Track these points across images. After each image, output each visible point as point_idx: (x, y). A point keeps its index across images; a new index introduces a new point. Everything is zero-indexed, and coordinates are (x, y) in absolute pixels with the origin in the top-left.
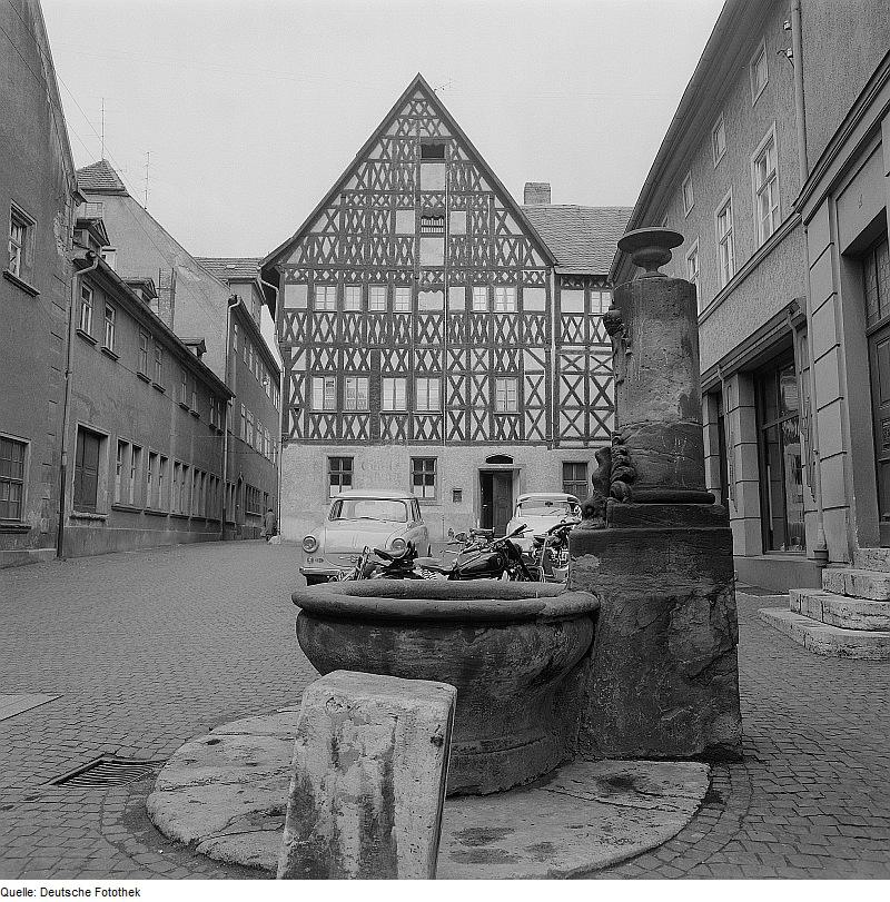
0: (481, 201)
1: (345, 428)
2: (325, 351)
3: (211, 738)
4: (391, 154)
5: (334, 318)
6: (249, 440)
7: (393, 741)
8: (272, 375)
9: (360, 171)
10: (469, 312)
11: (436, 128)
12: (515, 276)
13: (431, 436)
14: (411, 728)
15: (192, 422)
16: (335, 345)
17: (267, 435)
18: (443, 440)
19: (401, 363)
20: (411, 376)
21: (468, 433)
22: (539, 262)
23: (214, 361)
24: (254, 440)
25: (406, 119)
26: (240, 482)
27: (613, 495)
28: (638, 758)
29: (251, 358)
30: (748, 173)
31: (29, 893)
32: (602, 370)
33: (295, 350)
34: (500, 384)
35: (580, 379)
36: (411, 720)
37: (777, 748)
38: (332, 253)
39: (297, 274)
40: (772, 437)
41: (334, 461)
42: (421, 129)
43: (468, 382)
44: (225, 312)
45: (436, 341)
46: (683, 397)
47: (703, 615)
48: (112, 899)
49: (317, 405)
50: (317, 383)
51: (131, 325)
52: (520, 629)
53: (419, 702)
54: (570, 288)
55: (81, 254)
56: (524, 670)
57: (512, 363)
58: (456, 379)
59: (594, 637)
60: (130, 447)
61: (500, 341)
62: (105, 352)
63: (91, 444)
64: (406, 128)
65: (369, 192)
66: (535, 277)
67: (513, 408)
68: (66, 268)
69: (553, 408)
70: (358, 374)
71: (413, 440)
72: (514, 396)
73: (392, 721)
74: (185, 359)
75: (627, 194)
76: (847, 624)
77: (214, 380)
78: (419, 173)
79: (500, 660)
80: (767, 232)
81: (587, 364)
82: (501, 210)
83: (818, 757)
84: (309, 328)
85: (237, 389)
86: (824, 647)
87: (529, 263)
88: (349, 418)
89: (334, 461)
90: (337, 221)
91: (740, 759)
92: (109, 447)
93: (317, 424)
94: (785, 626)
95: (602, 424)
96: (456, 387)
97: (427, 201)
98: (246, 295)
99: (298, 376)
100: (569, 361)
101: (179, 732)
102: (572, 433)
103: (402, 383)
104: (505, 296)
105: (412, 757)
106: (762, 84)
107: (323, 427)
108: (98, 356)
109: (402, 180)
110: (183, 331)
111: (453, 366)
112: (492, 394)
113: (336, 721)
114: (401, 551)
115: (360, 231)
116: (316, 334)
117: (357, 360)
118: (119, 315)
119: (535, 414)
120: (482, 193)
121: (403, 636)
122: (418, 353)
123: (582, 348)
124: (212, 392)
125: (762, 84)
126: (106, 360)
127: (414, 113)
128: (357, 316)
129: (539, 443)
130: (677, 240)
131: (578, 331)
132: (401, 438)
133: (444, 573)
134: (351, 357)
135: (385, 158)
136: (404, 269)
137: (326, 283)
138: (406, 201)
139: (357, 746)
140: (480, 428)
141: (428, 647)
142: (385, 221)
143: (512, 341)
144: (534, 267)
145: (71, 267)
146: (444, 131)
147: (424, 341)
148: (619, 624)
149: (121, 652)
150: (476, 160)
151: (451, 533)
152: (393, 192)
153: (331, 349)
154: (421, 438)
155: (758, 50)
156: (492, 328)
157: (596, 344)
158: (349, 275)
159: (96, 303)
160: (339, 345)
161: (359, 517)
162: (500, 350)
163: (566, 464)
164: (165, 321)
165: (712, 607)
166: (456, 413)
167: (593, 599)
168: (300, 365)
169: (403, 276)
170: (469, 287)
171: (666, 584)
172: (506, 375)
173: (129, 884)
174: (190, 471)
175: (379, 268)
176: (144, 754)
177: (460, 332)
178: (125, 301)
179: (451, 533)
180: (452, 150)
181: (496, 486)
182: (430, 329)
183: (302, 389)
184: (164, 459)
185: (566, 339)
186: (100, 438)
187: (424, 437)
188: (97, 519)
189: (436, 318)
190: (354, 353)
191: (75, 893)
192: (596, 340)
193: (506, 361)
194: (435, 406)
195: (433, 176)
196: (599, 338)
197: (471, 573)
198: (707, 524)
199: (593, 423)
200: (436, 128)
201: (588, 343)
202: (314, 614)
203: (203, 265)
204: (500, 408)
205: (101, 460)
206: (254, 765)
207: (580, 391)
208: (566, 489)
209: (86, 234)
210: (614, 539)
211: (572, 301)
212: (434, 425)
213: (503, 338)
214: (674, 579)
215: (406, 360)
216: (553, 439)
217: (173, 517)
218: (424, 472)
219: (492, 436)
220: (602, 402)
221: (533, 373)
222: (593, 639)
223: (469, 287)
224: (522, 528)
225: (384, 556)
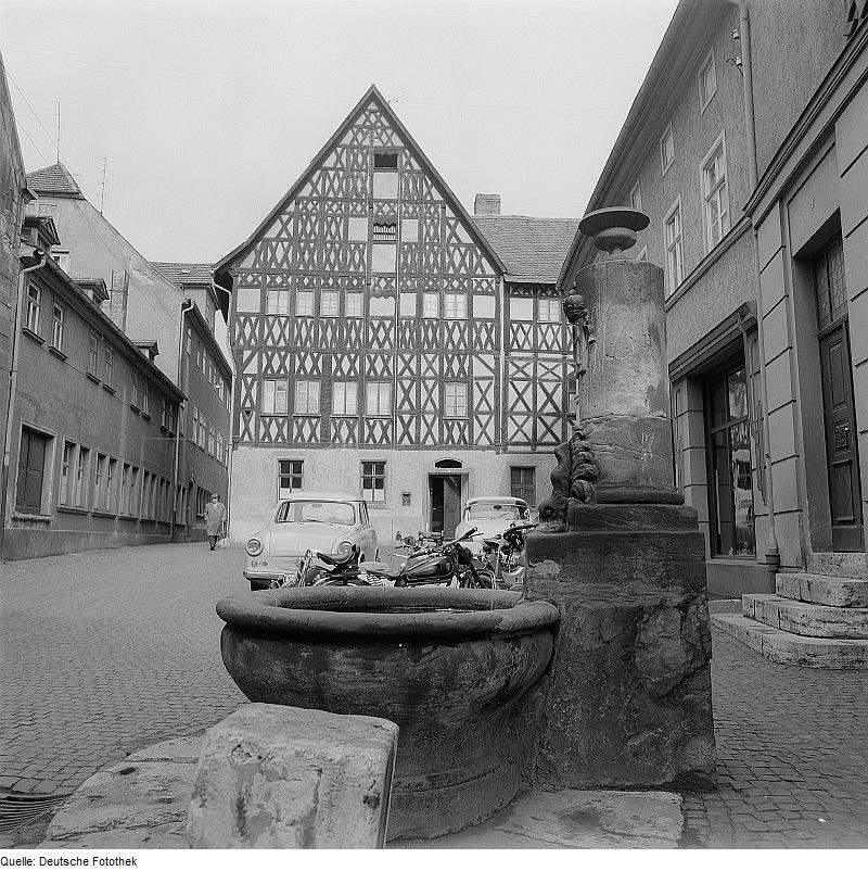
0: (432, 210)
1: (295, 431)
2: (276, 355)
3: (124, 766)
4: (344, 163)
5: (286, 323)
6: (201, 444)
7: (316, 801)
8: (223, 377)
9: (314, 179)
10: (419, 319)
11: (389, 139)
12: (465, 284)
13: (381, 440)
14: (339, 784)
15: (143, 423)
16: (287, 349)
17: (220, 439)
18: (394, 444)
19: (352, 368)
20: (362, 380)
21: (418, 437)
22: (489, 270)
23: (168, 364)
24: (207, 442)
25: (360, 129)
26: (191, 484)
27: (574, 495)
28: (602, 788)
29: (205, 363)
30: (697, 180)
31: (28, 862)
33: (247, 354)
34: (450, 389)
35: (528, 386)
36: (337, 775)
37: (754, 775)
38: (285, 258)
39: (250, 279)
40: (720, 441)
41: (284, 464)
42: (375, 139)
43: (419, 387)
44: (179, 316)
45: (387, 346)
46: (651, 389)
47: (674, 628)
48: (109, 868)
49: (268, 409)
50: (269, 386)
51: (80, 325)
52: (473, 646)
53: (349, 750)
54: (519, 296)
55: (29, 252)
56: (477, 693)
57: (462, 369)
58: (406, 384)
59: (554, 651)
60: (78, 448)
61: (450, 347)
62: (53, 351)
63: (36, 446)
64: (360, 137)
65: (323, 199)
66: (485, 285)
67: (462, 413)
68: (12, 266)
69: (502, 413)
70: (309, 377)
71: (363, 444)
72: (463, 402)
73: (315, 776)
74: (137, 362)
75: (571, 200)
76: (805, 631)
77: (167, 383)
78: (372, 180)
79: (450, 683)
80: (716, 237)
81: (535, 371)
82: (453, 219)
83: (776, 771)
84: (262, 332)
85: (190, 393)
86: (783, 656)
87: (479, 272)
88: (300, 421)
89: (284, 464)
90: (290, 227)
91: (714, 789)
92: (54, 450)
93: (267, 427)
94: (740, 633)
95: (549, 430)
96: (407, 392)
97: (380, 208)
98: (201, 300)
99: (249, 380)
100: (518, 368)
101: (91, 758)
102: (520, 438)
103: (353, 387)
104: (456, 303)
105: (340, 822)
106: (710, 92)
107: (274, 430)
108: (46, 356)
109: (355, 188)
110: (135, 333)
111: (403, 371)
112: (442, 399)
113: (244, 775)
114: (347, 553)
115: (313, 237)
116: (268, 338)
117: (309, 364)
118: (68, 313)
119: (484, 419)
120: (433, 202)
121: (338, 656)
122: (369, 357)
123: (530, 355)
124: (164, 395)
125: (710, 92)
126: (54, 360)
127: (368, 124)
128: (309, 321)
129: (488, 448)
130: (639, 222)
131: (527, 338)
132: (351, 441)
133: (391, 579)
134: (303, 361)
135: (339, 166)
136: (357, 275)
137: (279, 288)
138: (359, 208)
139: (270, 809)
140: (429, 432)
141: (367, 668)
142: (338, 227)
143: (462, 347)
144: (484, 275)
145: (18, 265)
146: (397, 142)
147: (375, 346)
148: (581, 638)
149: (44, 663)
150: (428, 170)
151: (399, 537)
152: (346, 199)
153: (283, 353)
154: (371, 442)
155: (707, 59)
156: (442, 335)
157: (544, 351)
158: (301, 281)
159: (43, 301)
160: (291, 349)
161: (296, 519)
162: (450, 356)
163: (514, 469)
164: (117, 323)
165: (683, 619)
166: (406, 418)
167: (553, 610)
168: (252, 368)
169: (355, 282)
170: (420, 293)
171: (633, 593)
172: (455, 380)
173: (126, 854)
174: (119, 465)
175: (332, 274)
176: (46, 788)
177: (411, 337)
178: (76, 302)
179: (399, 537)
180: (404, 160)
181: (444, 487)
182: (381, 334)
183: (254, 392)
184: (113, 461)
185: (515, 347)
186: (46, 438)
187: (374, 440)
188: (42, 521)
189: (388, 323)
190: (305, 357)
191: (73, 862)
192: (544, 348)
193: (456, 366)
194: (385, 411)
195: (386, 185)
196: (547, 345)
197: (422, 578)
198: (676, 527)
199: (541, 429)
200: (389, 139)
201: (536, 350)
202: (240, 628)
203: (159, 269)
204: (449, 413)
205: (47, 461)
206: (169, 801)
207: (528, 397)
208: (514, 493)
209: (35, 232)
210: (577, 542)
211: (521, 308)
212: (384, 429)
213: (453, 344)
214: (642, 588)
215: (357, 365)
216: (501, 444)
217: (121, 519)
218: (374, 476)
219: (441, 440)
220: (549, 408)
221: (483, 378)
222: (553, 654)
223: (420, 293)
224: (473, 531)
225: (327, 560)
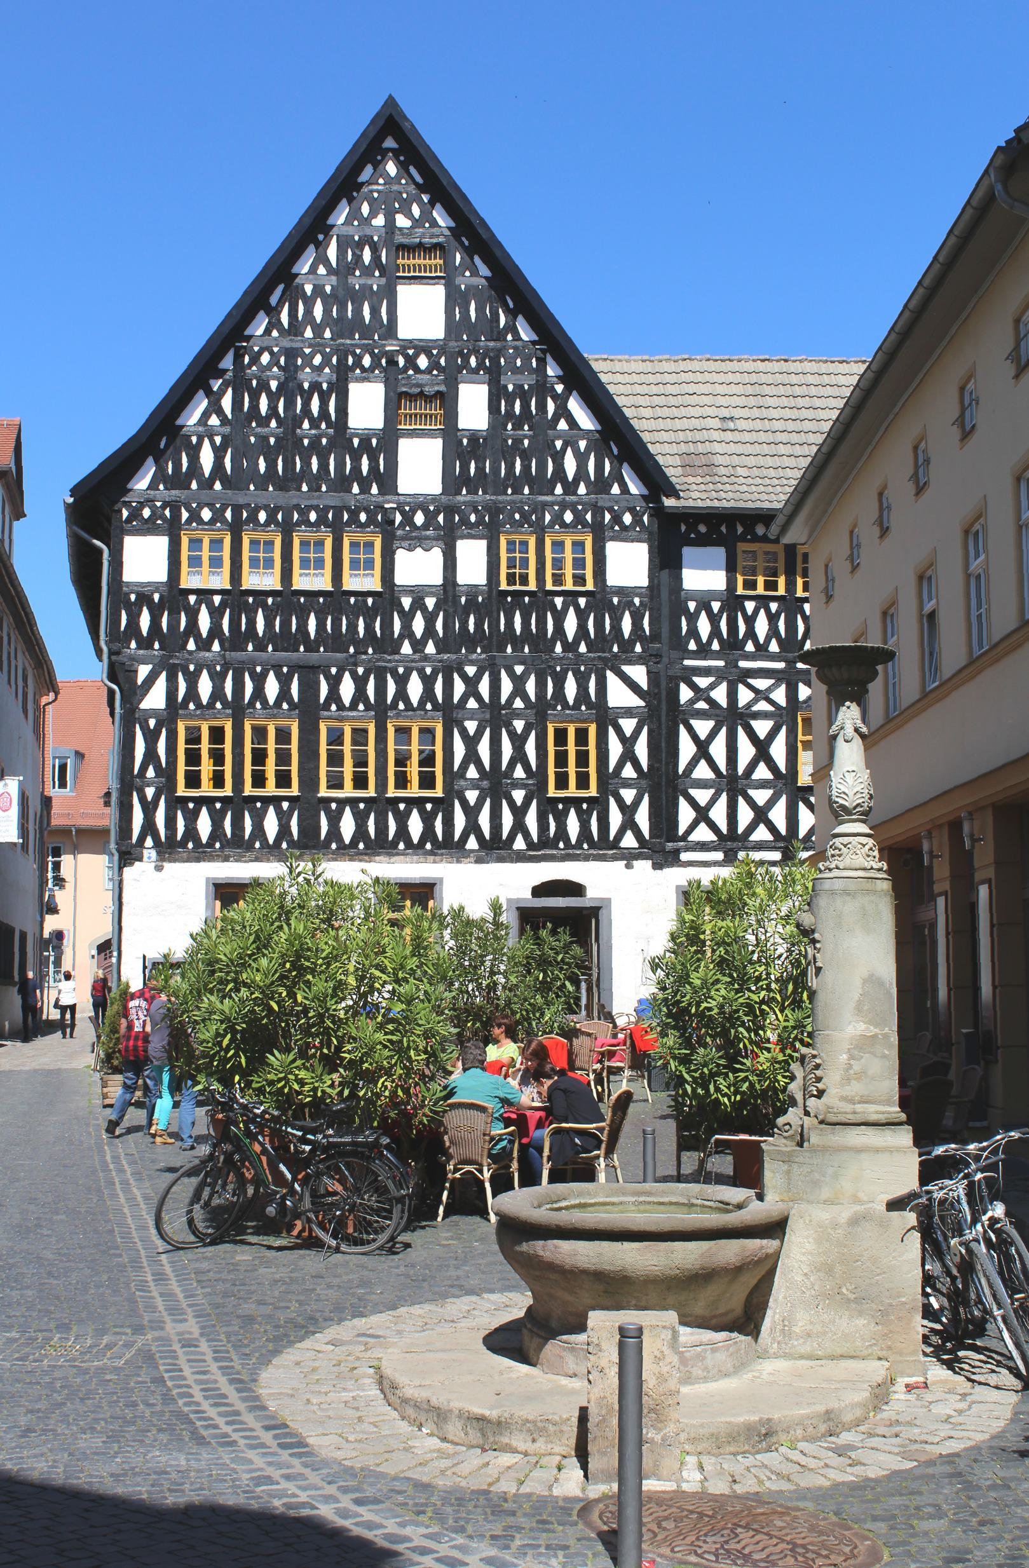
32: (763, 706)
33: (143, 671)
82: (628, 712)
189: (430, 602)
207: (718, 750)
